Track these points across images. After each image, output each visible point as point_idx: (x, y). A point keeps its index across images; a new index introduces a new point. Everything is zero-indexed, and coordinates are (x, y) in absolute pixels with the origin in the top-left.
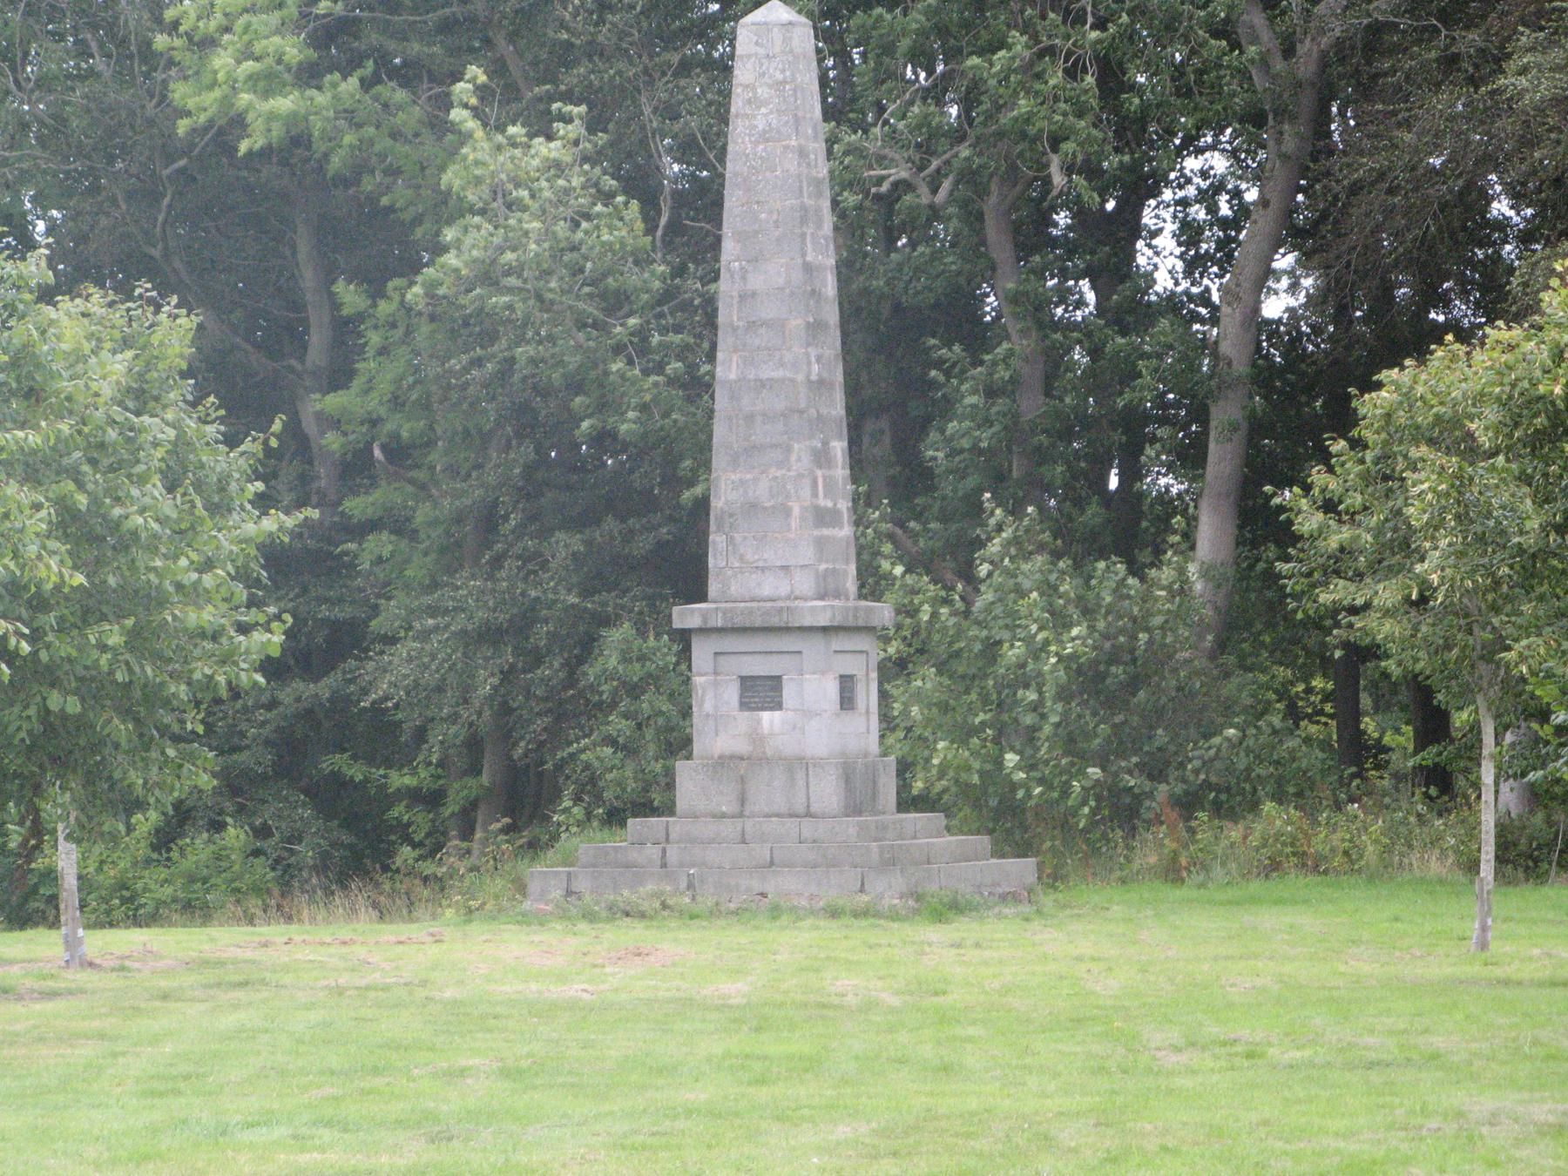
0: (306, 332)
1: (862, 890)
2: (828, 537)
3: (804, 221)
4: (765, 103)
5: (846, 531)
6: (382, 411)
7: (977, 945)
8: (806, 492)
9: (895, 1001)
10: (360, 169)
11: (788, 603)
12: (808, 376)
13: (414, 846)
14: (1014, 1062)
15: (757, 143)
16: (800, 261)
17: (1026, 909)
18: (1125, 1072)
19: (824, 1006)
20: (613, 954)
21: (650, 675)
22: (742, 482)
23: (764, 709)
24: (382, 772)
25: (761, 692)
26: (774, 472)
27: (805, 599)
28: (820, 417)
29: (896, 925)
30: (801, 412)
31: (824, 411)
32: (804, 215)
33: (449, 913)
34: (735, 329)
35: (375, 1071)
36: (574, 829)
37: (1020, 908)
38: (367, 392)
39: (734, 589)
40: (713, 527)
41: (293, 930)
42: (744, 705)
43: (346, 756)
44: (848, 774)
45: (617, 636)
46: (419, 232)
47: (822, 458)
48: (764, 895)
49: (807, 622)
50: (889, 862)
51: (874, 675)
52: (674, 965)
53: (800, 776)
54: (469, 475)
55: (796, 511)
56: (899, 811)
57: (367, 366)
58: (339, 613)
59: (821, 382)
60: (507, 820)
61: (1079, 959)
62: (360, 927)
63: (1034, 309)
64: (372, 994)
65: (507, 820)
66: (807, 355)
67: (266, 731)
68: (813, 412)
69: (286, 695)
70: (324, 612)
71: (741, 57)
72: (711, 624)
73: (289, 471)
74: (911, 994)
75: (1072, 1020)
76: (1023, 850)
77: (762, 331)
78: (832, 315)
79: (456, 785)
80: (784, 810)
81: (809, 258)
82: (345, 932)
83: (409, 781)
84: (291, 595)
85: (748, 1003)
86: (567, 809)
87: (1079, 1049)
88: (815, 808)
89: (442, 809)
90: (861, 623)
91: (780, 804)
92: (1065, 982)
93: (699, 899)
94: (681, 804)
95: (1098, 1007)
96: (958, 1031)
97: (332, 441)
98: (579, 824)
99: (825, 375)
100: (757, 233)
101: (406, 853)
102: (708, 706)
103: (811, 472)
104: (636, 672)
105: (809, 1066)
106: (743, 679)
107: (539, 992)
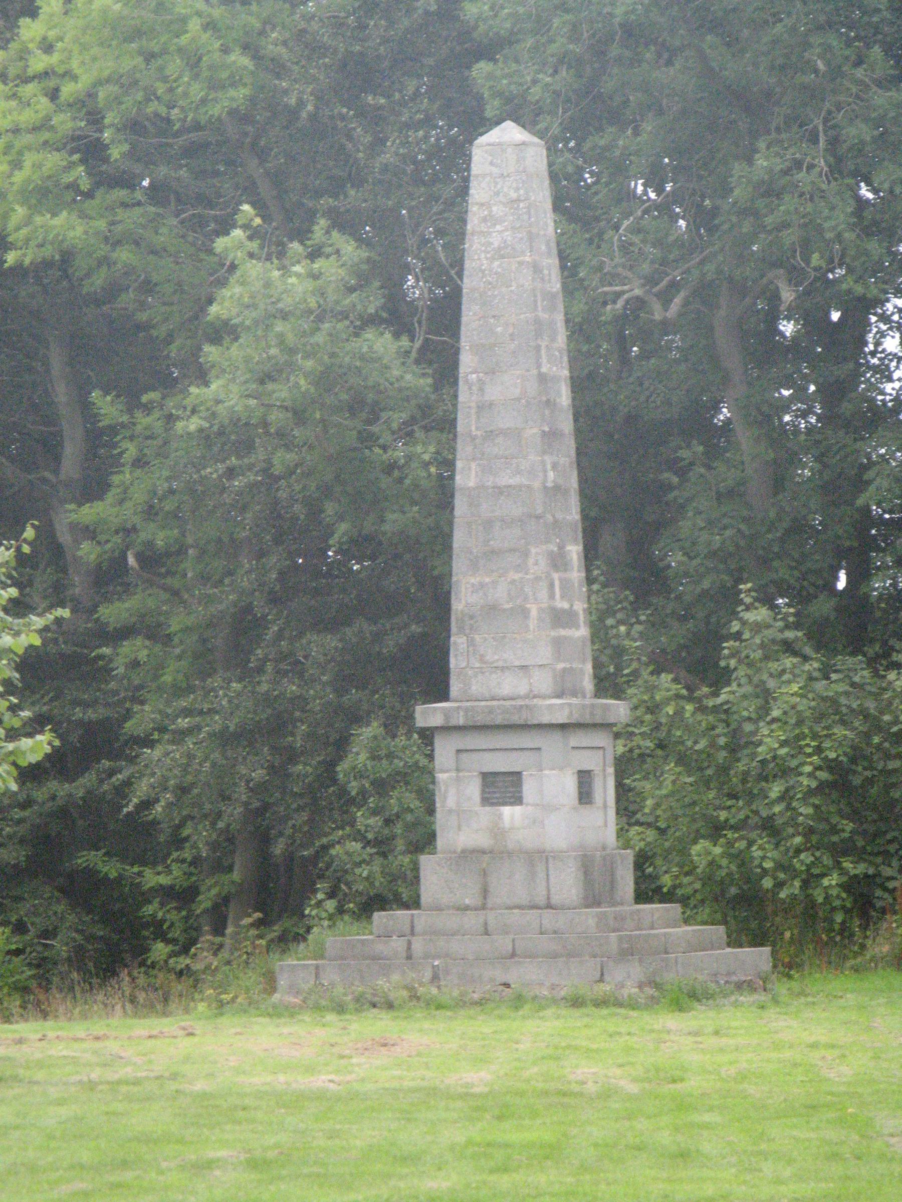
0: (61, 444)
1: (601, 980)
2: (565, 638)
3: (538, 334)
4: (497, 221)
5: (582, 632)
6: (137, 520)
7: (716, 1033)
8: (543, 594)
9: (633, 1088)
10: (113, 291)
11: (527, 702)
12: (544, 484)
13: (167, 941)
14: (750, 1148)
15: (493, 259)
16: (535, 372)
17: (762, 997)
18: (858, 1158)
19: (565, 1094)
20: (359, 1045)
21: (398, 773)
22: (482, 585)
23: (505, 804)
24: (136, 869)
25: (502, 788)
26: (514, 576)
27: (544, 697)
28: (556, 521)
29: (634, 1014)
30: (538, 517)
31: (560, 516)
32: (539, 327)
33: (201, 1007)
34: (473, 438)
35: (125, 1164)
36: (326, 923)
37: (756, 996)
38: (121, 502)
39: (475, 688)
40: (454, 628)
41: (50, 1027)
42: (486, 801)
43: (100, 853)
44: (586, 865)
45: (368, 732)
46: (173, 350)
47: (558, 561)
48: (507, 985)
49: (546, 719)
50: (627, 953)
51: (611, 770)
52: (419, 1055)
53: (540, 868)
54: (221, 581)
55: (534, 612)
56: (637, 903)
57: (122, 478)
58: (91, 715)
59: (557, 488)
60: (258, 915)
61: (814, 1046)
62: (114, 1022)
63: (765, 417)
64: (124, 1089)
65: (258, 915)
66: (543, 462)
67: (22, 830)
68: (549, 517)
69: (40, 795)
70: (78, 713)
71: (477, 176)
72: (453, 722)
73: (44, 578)
74: (650, 1081)
75: (807, 1107)
76: (758, 940)
77: (500, 440)
78: (567, 425)
79: (209, 882)
80: (524, 902)
81: (544, 370)
82: (98, 1027)
83: (164, 880)
84: (46, 699)
85: (490, 1092)
86: (320, 905)
87: (812, 1135)
88: (555, 900)
89: (193, 906)
90: (598, 720)
91: (522, 897)
92: (800, 1069)
93: (444, 989)
94: (425, 898)
95: (832, 1094)
96: (696, 1118)
97: (88, 551)
98: (331, 917)
99: (560, 481)
100: (495, 345)
101: (160, 950)
102: (451, 802)
103: (548, 575)
104: (384, 769)
105: (550, 1153)
106: (485, 776)
107: (286, 1083)
